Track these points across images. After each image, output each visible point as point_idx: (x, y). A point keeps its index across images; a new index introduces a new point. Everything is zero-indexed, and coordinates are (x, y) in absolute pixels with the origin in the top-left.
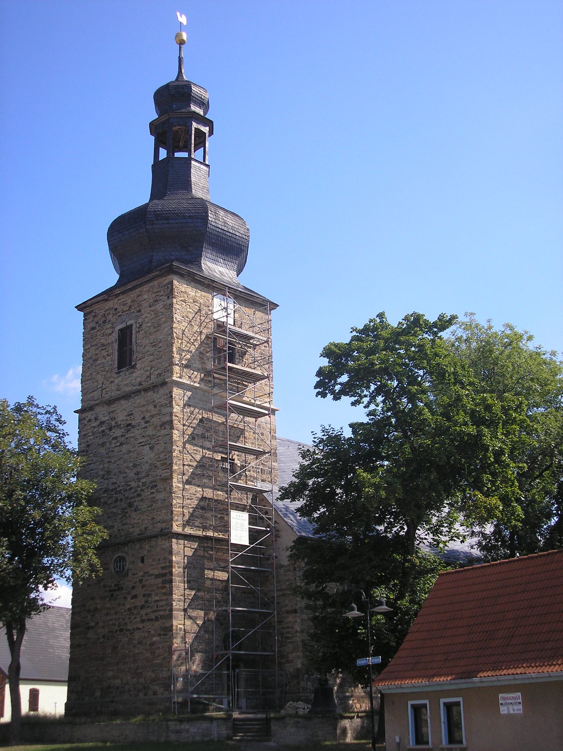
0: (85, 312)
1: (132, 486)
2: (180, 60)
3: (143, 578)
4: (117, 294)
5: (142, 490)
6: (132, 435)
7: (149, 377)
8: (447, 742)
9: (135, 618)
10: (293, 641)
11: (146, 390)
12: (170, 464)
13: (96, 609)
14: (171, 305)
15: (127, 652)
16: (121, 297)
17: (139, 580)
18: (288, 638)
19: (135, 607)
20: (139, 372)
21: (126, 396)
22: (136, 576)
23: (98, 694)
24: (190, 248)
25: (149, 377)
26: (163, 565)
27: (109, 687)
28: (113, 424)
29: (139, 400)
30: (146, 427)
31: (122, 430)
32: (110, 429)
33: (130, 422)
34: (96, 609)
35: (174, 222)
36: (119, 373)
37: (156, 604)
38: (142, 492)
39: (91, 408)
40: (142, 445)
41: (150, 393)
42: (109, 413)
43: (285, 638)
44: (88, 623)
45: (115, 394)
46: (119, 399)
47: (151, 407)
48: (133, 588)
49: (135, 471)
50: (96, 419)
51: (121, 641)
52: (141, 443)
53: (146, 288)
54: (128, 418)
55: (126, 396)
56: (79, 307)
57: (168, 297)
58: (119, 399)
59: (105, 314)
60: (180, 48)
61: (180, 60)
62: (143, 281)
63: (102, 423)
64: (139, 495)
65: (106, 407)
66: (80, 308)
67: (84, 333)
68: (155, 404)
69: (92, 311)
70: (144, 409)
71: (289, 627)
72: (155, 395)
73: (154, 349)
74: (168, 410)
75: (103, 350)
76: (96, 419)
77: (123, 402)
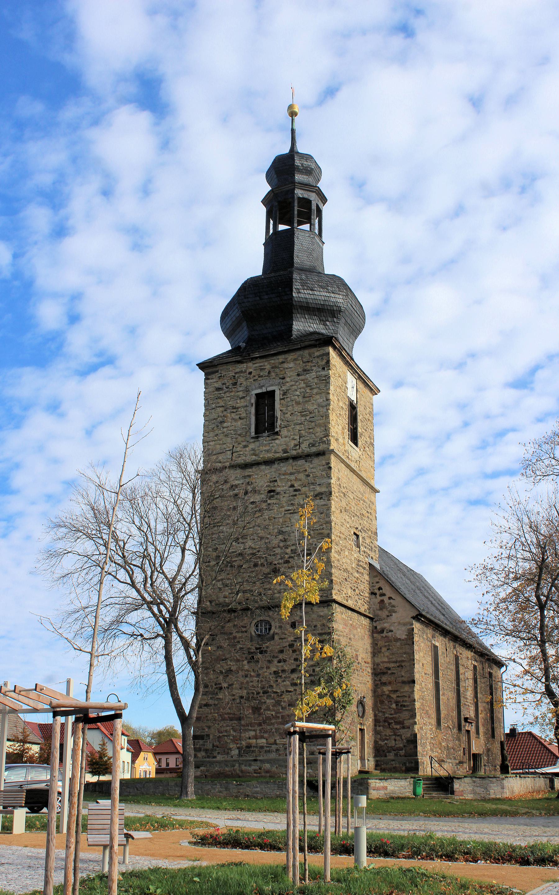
0: (207, 371)
1: (277, 552)
2: (293, 131)
3: (294, 643)
4: (254, 358)
5: (290, 557)
6: (275, 501)
7: (299, 444)
8: (113, 785)
9: (284, 681)
10: (409, 708)
11: (295, 458)
12: (329, 534)
13: (230, 671)
14: (328, 377)
15: (273, 713)
16: (257, 361)
17: (289, 645)
18: (404, 706)
19: (283, 671)
20: (284, 439)
21: (269, 462)
22: (284, 640)
23: (235, 752)
24: (328, 323)
25: (299, 444)
26: (321, 631)
27: (249, 746)
28: (249, 488)
29: (285, 467)
30: (295, 495)
31: (263, 496)
32: (246, 493)
33: (273, 489)
34: (230, 671)
35: (318, 293)
36: (257, 438)
37: (311, 669)
38: (290, 560)
39: (216, 470)
40: (291, 513)
41: (301, 462)
42: (245, 477)
43: (401, 706)
44: (220, 684)
45: (250, 458)
46: (257, 464)
47: (302, 476)
48: (282, 651)
49: (281, 537)
50: (226, 482)
51: (265, 702)
52: (289, 510)
53: (291, 356)
54: (272, 484)
55: (269, 462)
56: (202, 366)
57: (324, 369)
58: (257, 464)
59: (234, 376)
60: (292, 120)
61: (293, 131)
62: (291, 349)
63: (233, 487)
64: (287, 562)
65: (239, 471)
66: (202, 366)
67: (205, 393)
68: (307, 473)
69: (217, 371)
70: (293, 477)
71: (405, 696)
72: (308, 464)
73: (303, 418)
74: (325, 480)
75: (233, 412)
76: (226, 482)
77: (263, 467)
